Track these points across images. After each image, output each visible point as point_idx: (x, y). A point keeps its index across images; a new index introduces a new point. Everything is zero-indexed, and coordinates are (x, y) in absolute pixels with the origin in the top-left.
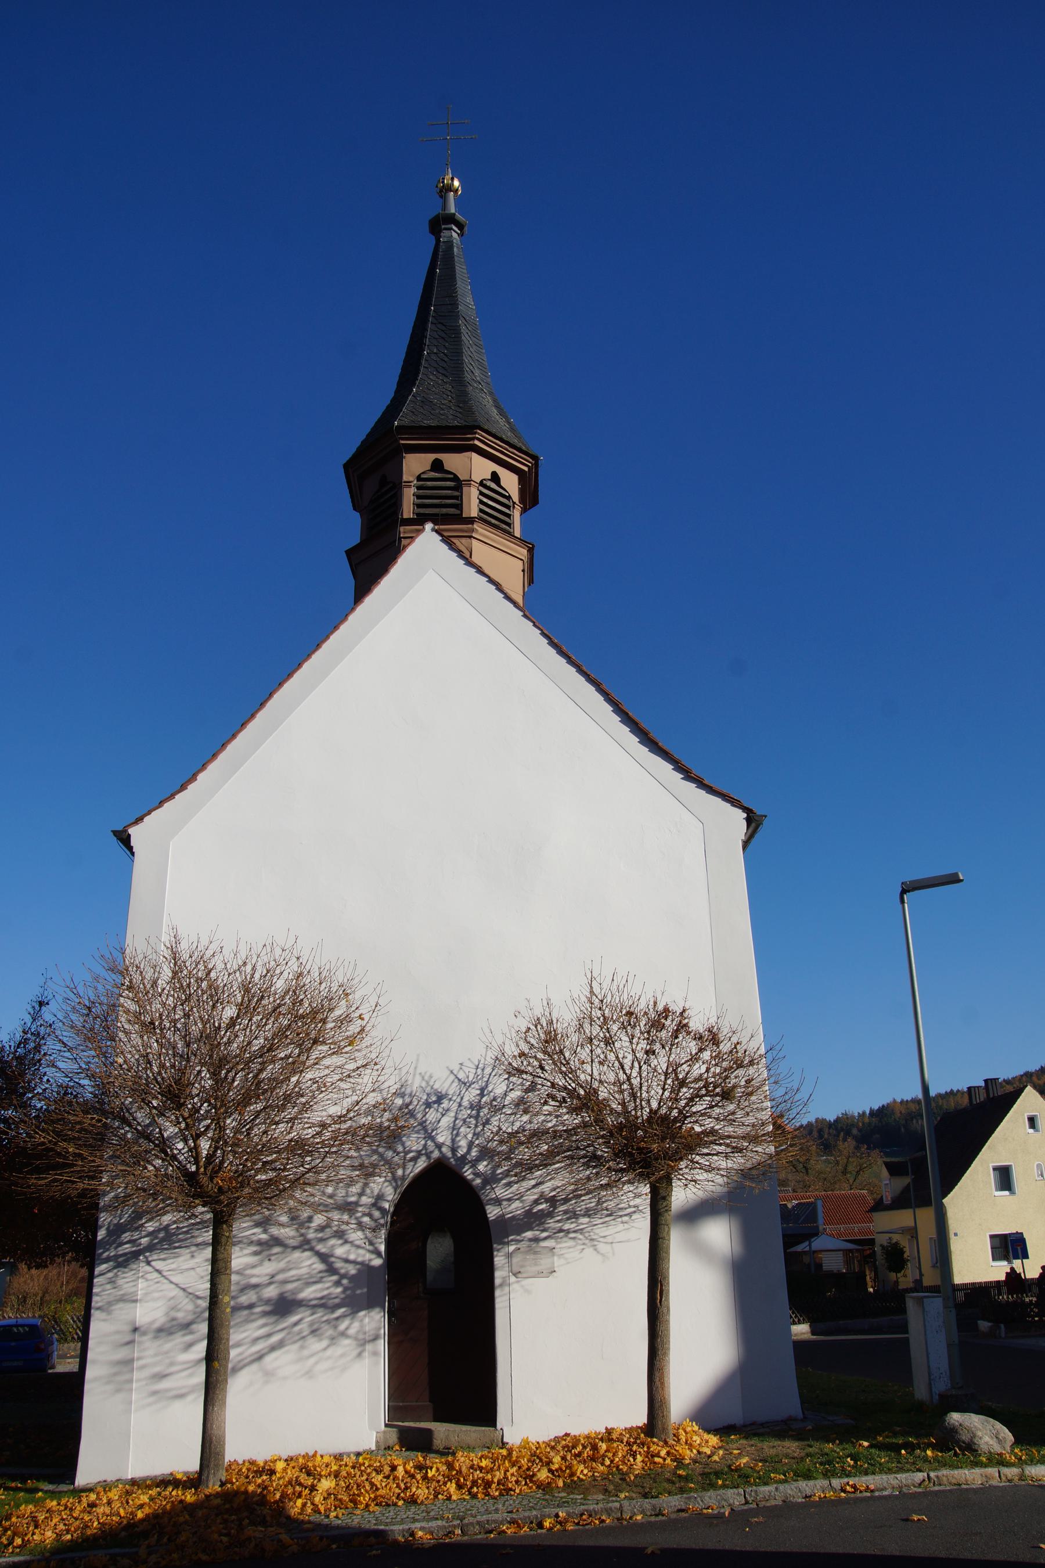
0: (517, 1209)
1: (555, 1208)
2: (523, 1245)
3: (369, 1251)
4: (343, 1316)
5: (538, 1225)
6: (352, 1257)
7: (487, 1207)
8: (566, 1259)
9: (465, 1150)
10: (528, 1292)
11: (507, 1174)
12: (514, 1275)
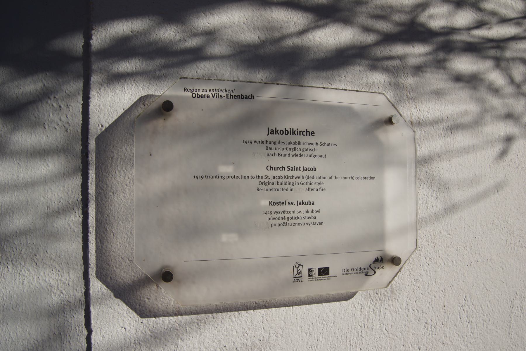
2: (199, 94)
8: (442, 186)
12: (127, 293)
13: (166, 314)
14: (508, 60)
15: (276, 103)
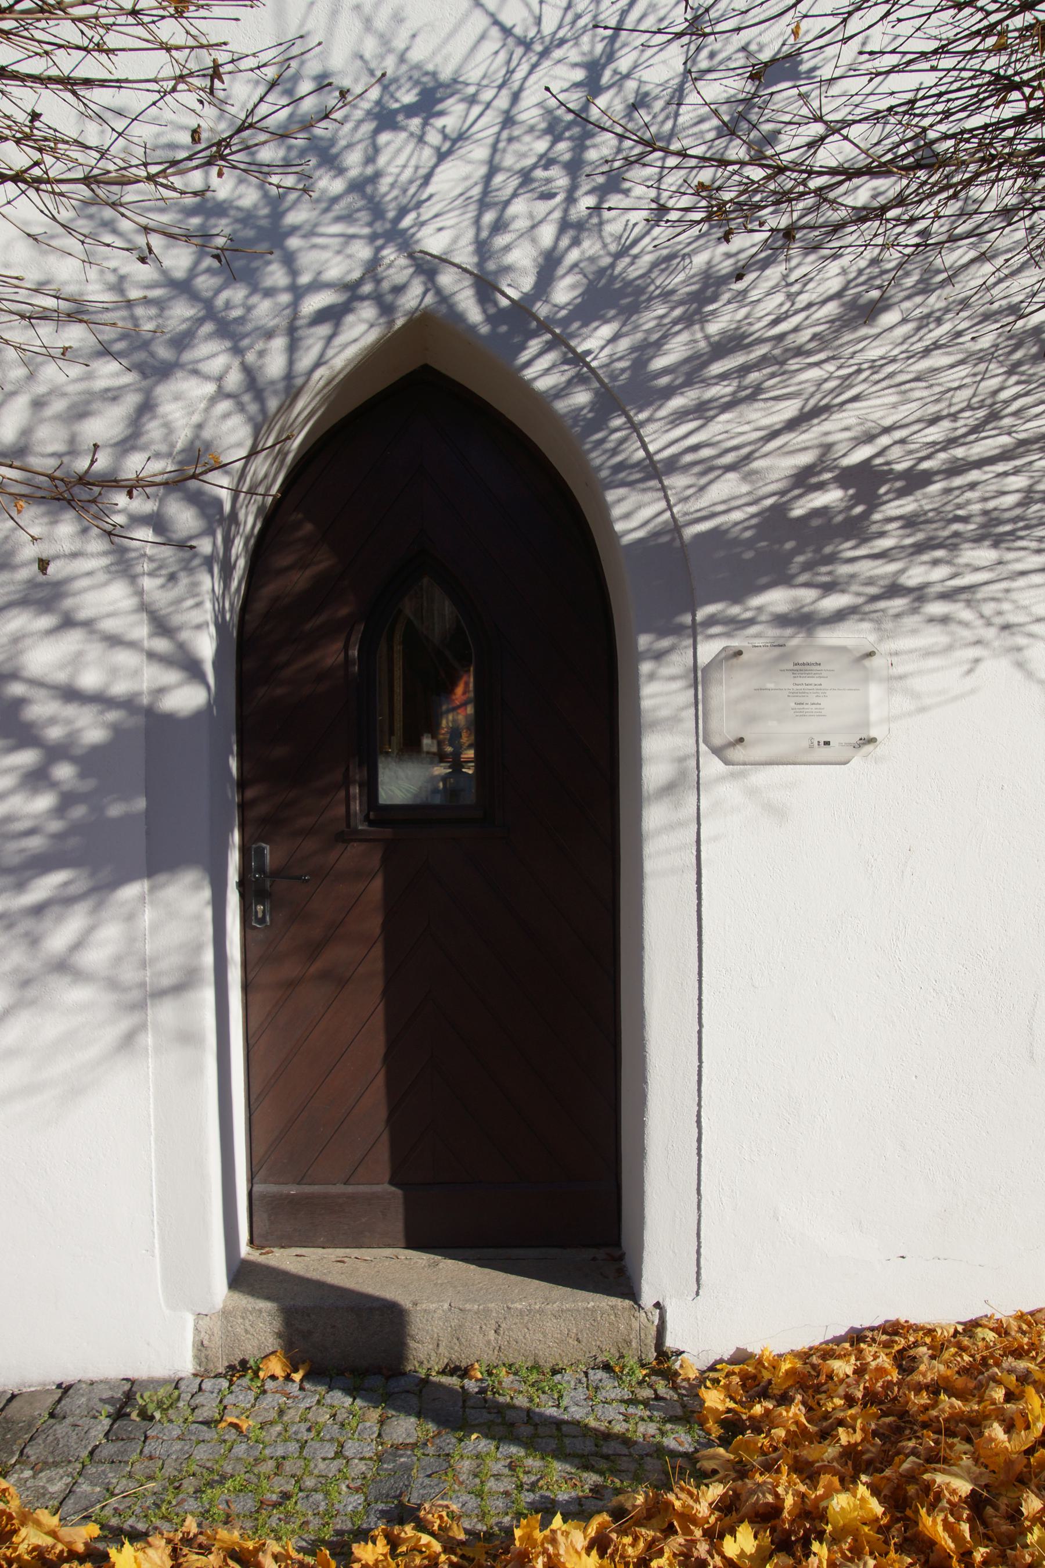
0: (729, 505)
1: (874, 503)
2: (754, 641)
3: (152, 656)
4: (64, 901)
5: (808, 567)
6: (90, 680)
7: (611, 496)
8: (915, 695)
9: (527, 283)
10: (777, 812)
11: (692, 370)
12: (717, 752)
13: (738, 764)
14: (978, 601)
15: (798, 647)
